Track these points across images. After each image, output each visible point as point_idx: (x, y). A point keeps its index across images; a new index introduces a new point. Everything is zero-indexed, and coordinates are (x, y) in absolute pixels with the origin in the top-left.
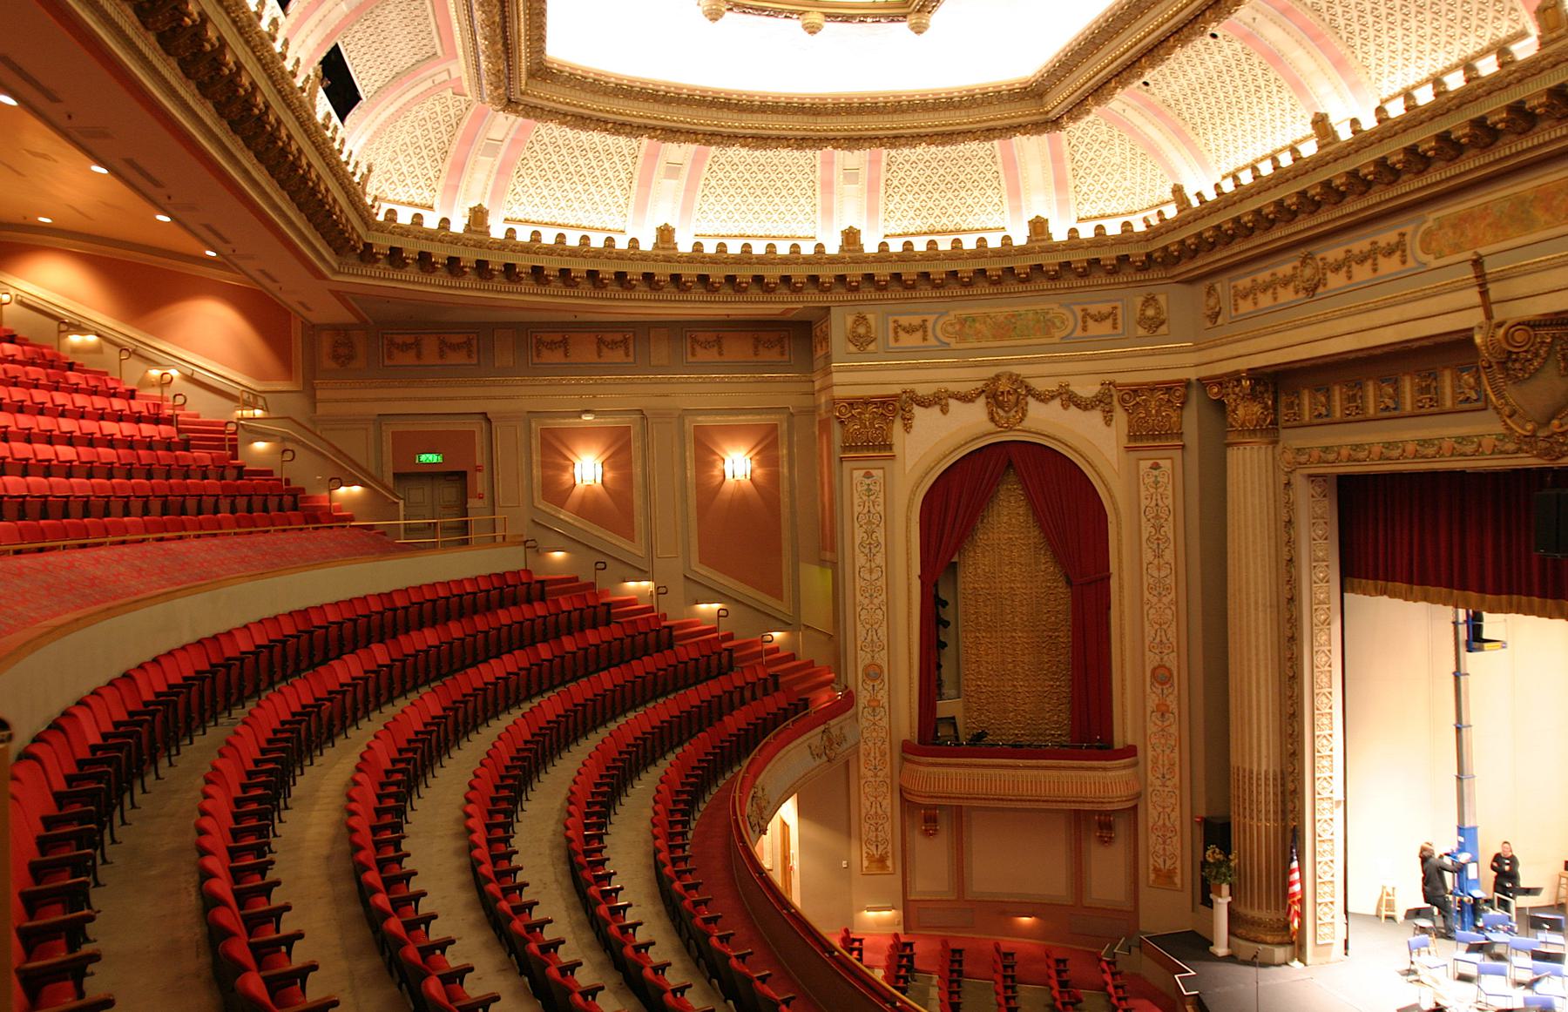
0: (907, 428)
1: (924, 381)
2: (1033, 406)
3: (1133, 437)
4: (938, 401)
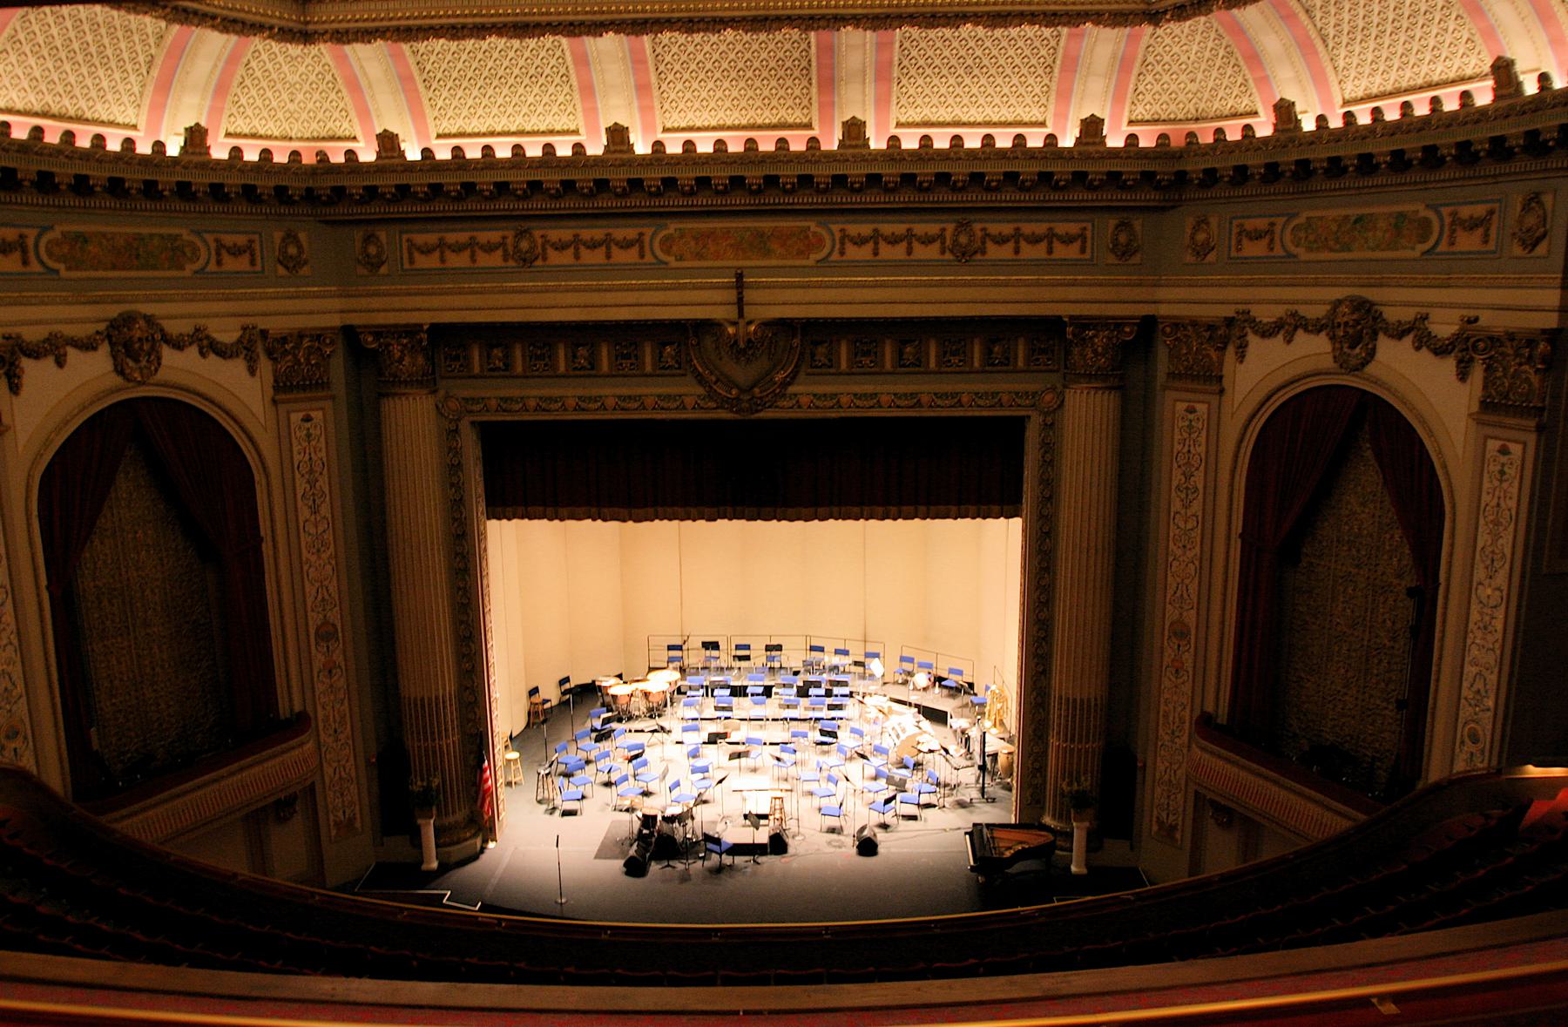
0: (1241, 357)
1: (1268, 303)
2: (168, 354)
3: (277, 388)
4: (1288, 326)
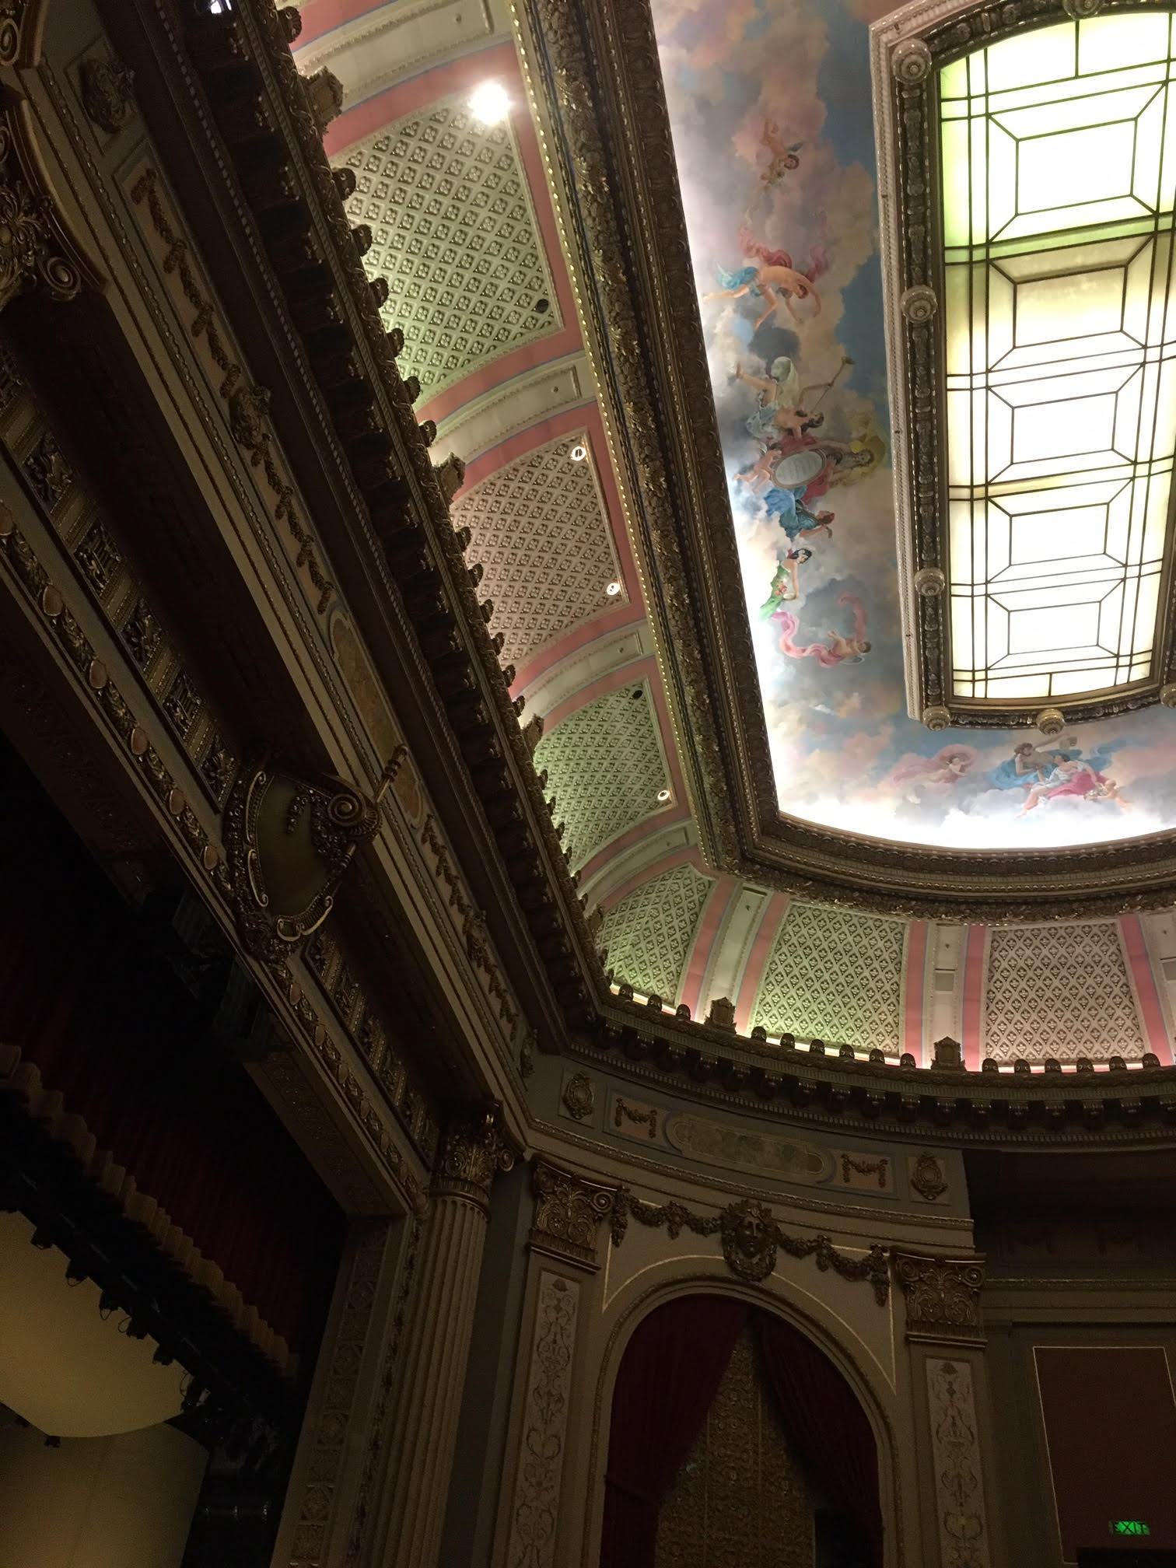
3: (911, 1324)
4: (673, 1219)
